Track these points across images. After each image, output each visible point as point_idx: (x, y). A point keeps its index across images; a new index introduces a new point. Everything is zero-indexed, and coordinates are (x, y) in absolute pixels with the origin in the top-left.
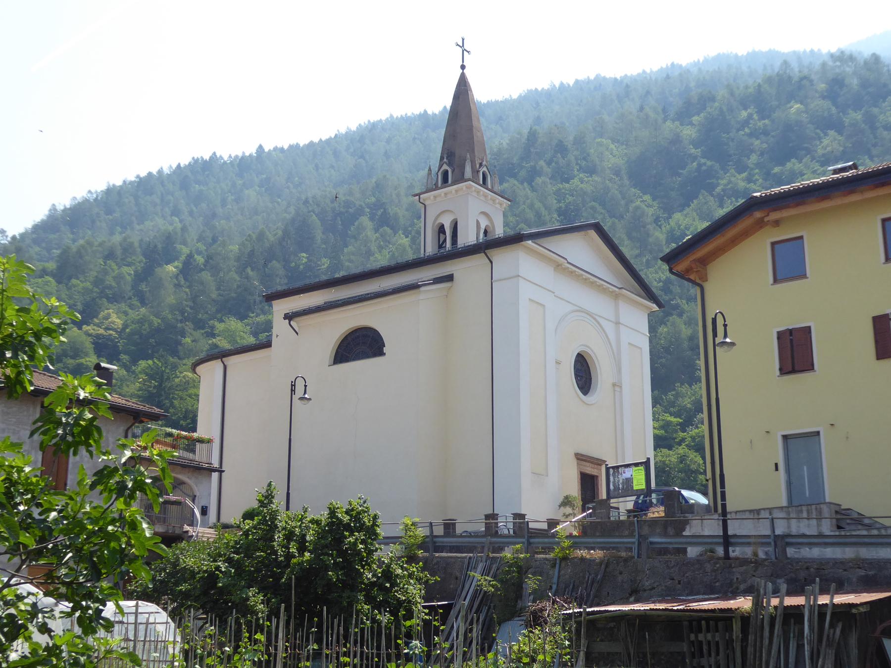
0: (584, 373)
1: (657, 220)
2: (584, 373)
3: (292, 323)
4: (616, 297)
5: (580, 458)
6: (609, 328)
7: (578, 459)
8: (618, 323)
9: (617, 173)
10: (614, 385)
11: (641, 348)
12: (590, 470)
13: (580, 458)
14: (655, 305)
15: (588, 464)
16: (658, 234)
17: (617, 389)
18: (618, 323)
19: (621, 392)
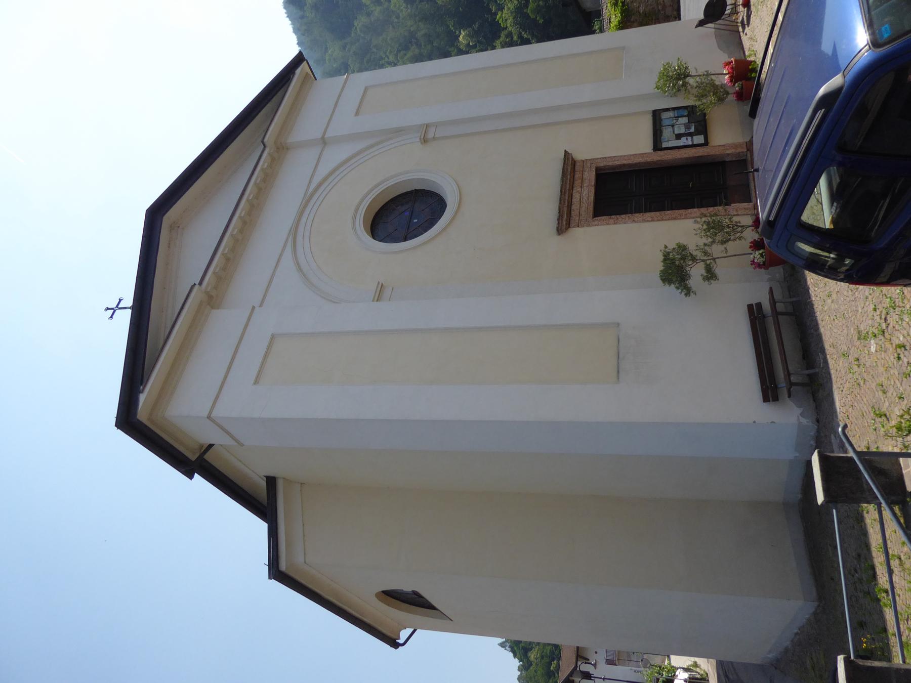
0: (405, 213)
1: (369, 14)
2: (405, 213)
3: (401, 641)
4: (282, 149)
5: (565, 222)
6: (335, 156)
7: (568, 226)
8: (324, 142)
9: (344, 47)
10: (425, 141)
11: (366, 89)
12: (585, 194)
13: (565, 222)
14: (298, 71)
15: (576, 196)
16: (376, 13)
17: (430, 135)
18: (324, 142)
19: (436, 125)
